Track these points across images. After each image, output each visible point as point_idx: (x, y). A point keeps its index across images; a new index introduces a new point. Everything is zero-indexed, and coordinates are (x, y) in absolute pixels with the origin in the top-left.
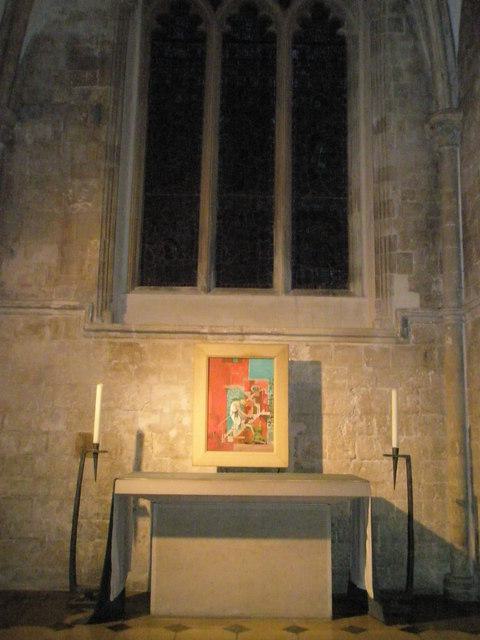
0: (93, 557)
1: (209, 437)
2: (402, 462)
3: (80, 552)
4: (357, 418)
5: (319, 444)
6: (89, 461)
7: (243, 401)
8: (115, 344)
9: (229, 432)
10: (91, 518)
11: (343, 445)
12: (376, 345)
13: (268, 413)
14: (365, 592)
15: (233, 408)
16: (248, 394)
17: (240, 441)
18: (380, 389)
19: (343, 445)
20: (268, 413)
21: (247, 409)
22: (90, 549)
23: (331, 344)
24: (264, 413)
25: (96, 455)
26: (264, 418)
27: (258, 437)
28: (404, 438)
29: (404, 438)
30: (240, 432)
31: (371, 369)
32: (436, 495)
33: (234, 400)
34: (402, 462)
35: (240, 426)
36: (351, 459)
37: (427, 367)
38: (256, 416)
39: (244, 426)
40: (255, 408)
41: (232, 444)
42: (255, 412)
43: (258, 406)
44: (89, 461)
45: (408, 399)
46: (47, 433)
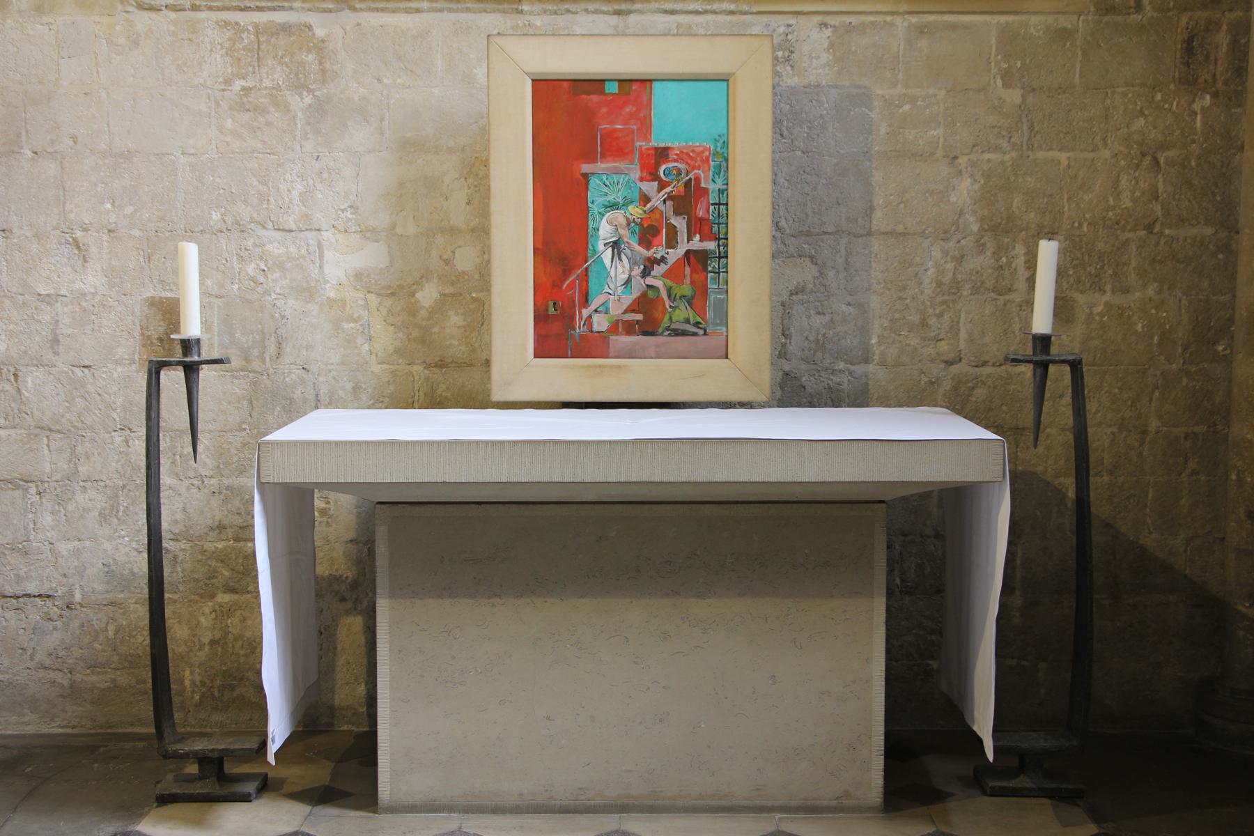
0: (213, 643)
1: (541, 318)
2: (1060, 376)
3: (177, 631)
4: (968, 242)
5: (599, 813)
6: (173, 380)
7: (635, 211)
8: (236, 26)
9: (595, 303)
10: (200, 538)
11: (924, 324)
12: (1034, 19)
13: (711, 245)
14: (980, 741)
15: (604, 230)
16: (650, 187)
17: (630, 328)
18: (1040, 155)
19: (924, 324)
20: (711, 245)
21: (647, 234)
22: (205, 621)
23: (898, 20)
24: (697, 244)
25: (191, 370)
26: (697, 259)
27: (682, 313)
28: (1094, 303)
29: (1094, 303)
30: (628, 300)
31: (1014, 96)
32: (1192, 465)
33: (613, 206)
34: (1060, 376)
35: (628, 282)
36: (949, 363)
37: (1190, 84)
38: (675, 255)
39: (638, 285)
40: (672, 231)
41: (603, 337)
42: (672, 243)
43: (680, 223)
44: (173, 380)
45: (1124, 181)
46: (49, 299)
